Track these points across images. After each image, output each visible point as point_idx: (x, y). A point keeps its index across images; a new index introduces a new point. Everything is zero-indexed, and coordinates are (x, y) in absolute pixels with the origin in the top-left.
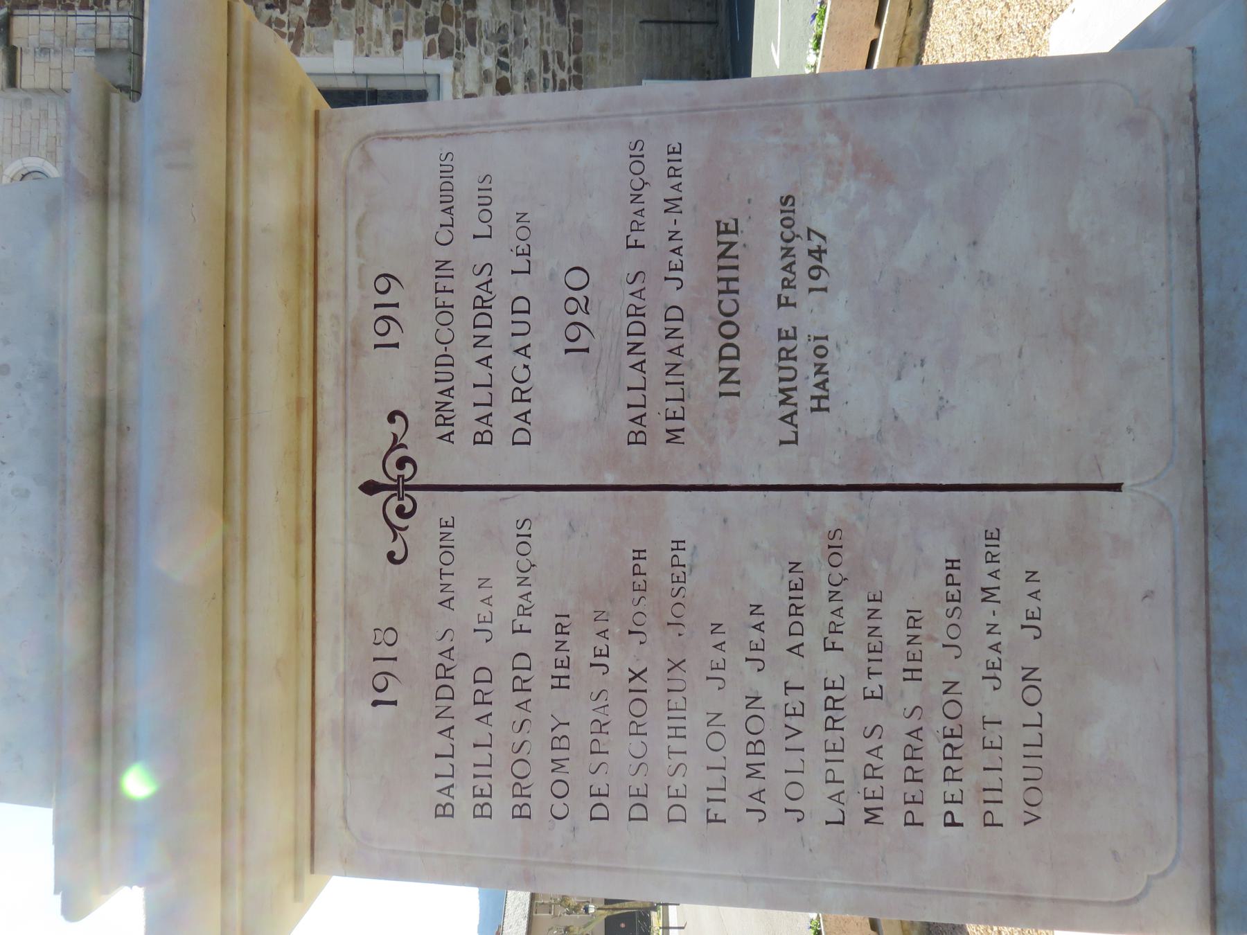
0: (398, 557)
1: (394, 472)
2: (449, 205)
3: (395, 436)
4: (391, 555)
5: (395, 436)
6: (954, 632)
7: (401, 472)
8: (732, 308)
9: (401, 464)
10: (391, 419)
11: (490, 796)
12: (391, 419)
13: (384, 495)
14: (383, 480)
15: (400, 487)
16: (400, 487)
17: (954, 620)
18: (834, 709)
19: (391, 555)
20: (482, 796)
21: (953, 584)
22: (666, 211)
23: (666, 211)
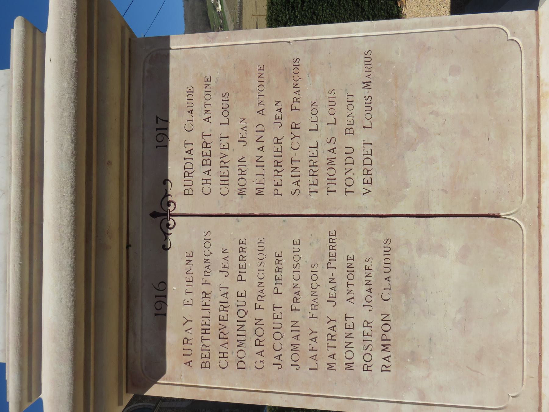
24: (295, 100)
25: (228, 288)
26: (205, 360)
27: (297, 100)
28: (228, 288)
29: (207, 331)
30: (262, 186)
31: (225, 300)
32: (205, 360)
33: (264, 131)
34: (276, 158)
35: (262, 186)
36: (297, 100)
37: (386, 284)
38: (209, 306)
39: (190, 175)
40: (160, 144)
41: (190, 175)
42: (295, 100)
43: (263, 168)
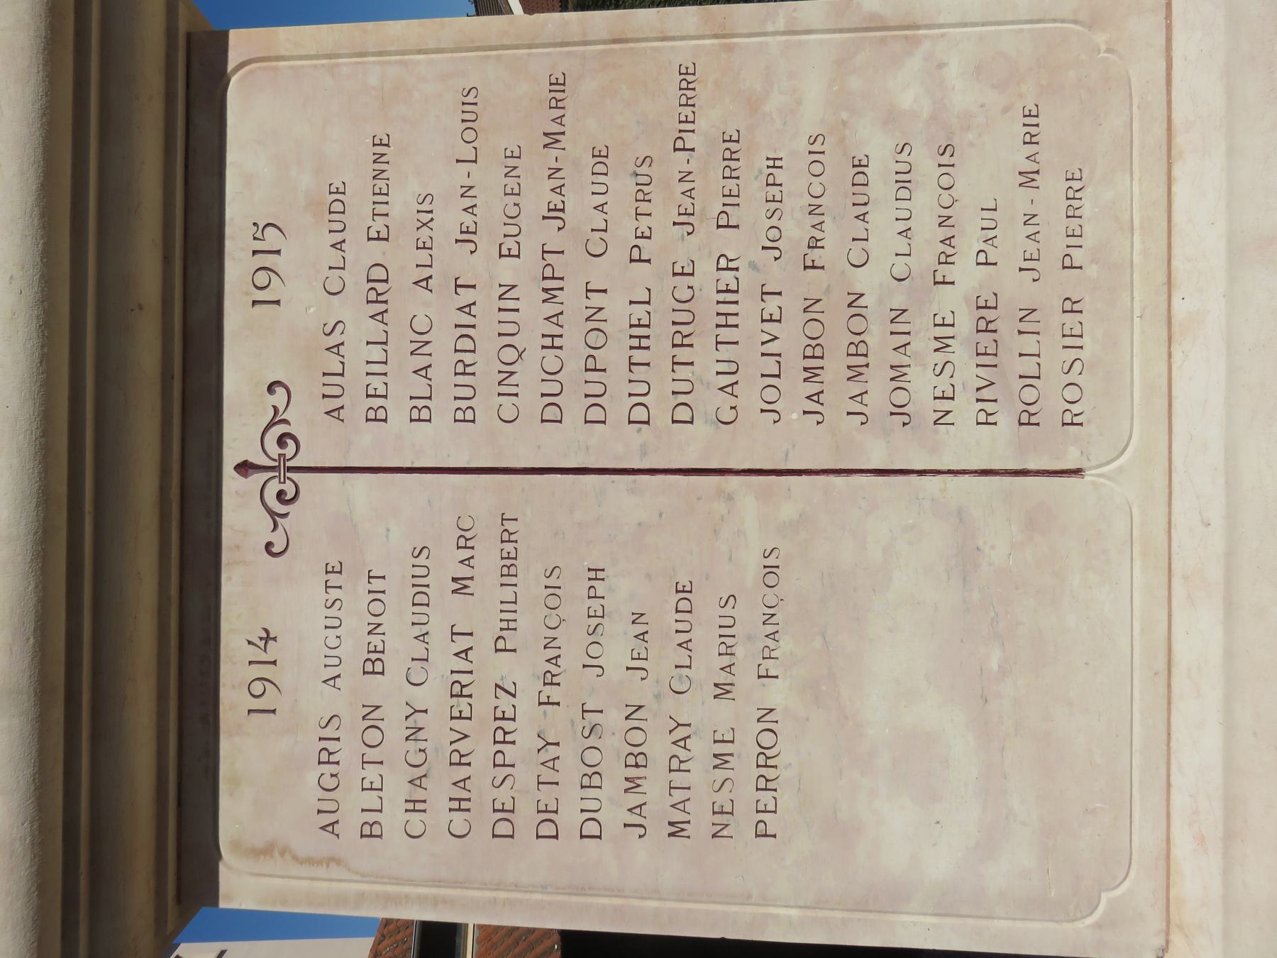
0: (275, 550)
1: (274, 450)
2: (332, 818)
3: (276, 409)
4: (269, 545)
5: (276, 409)
6: (774, 234)
7: (282, 487)
8: (687, 294)
9: (281, 441)
10: (271, 389)
11: (383, 652)
12: (271, 389)
13: (258, 478)
14: (262, 460)
15: (282, 468)
16: (282, 468)
17: (774, 221)
18: (766, 766)
19: (269, 545)
20: (375, 651)
21: (774, 184)
22: (715, 697)
23: (715, 697)
24: (943, 259)
25: (763, 354)
26: (508, 562)
27: (814, 244)
28: (763, 354)
29: (731, 320)
30: (862, 361)
31: (464, 665)
32: (508, 562)
33: (385, 363)
34: (553, 94)
35: (862, 361)
36: (814, 244)
37: (334, 257)
38: (648, 326)
39: (380, 298)
40: (261, 296)
41: (380, 298)
42: (943, 259)
43: (777, 358)
